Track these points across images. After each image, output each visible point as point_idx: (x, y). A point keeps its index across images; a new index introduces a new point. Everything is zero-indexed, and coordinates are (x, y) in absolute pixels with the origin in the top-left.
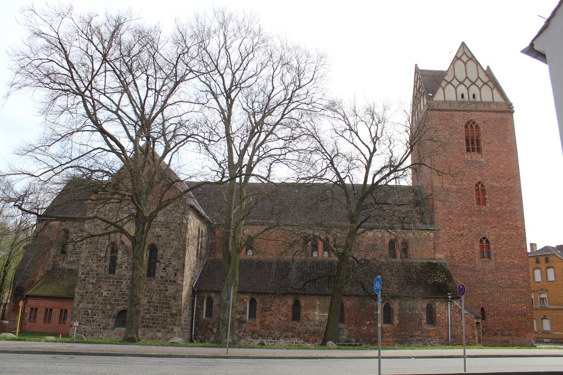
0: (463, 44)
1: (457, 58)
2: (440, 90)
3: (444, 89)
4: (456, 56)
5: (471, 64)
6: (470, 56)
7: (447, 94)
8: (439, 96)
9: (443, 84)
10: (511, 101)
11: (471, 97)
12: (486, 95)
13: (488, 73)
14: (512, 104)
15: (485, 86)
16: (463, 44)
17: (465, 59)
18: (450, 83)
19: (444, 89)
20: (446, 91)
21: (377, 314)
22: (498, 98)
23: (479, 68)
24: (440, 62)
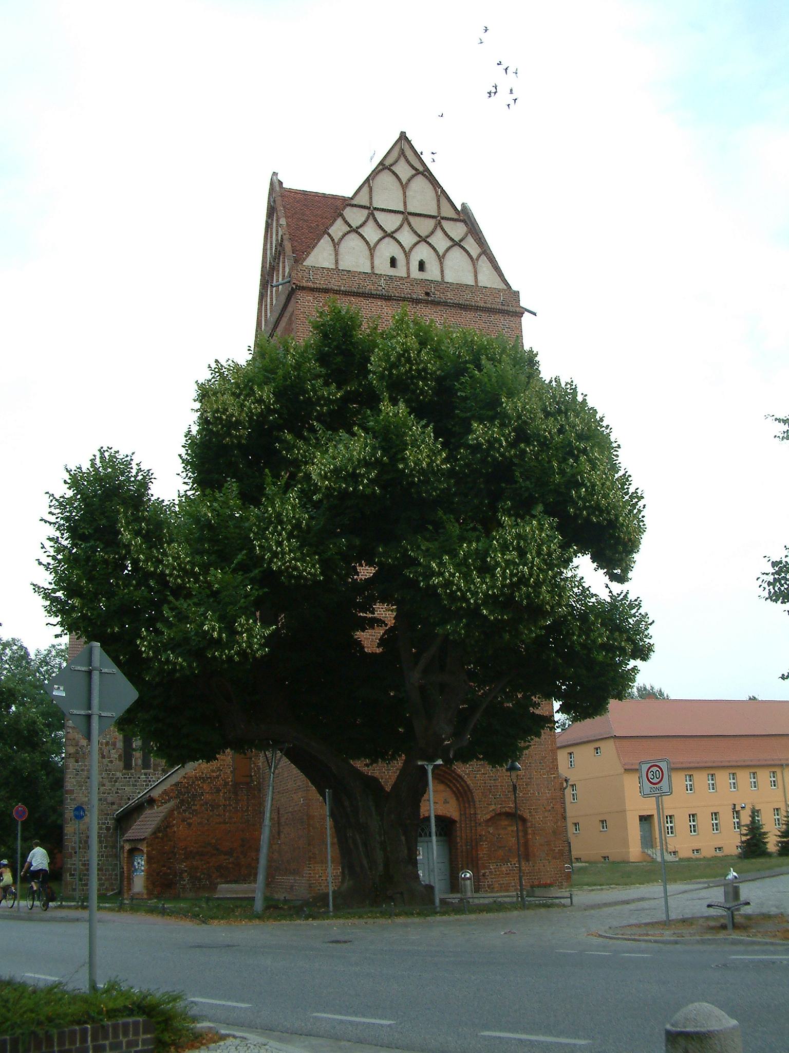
0: (403, 137)
1: (383, 167)
2: (325, 242)
3: (336, 245)
4: (381, 163)
5: (420, 183)
6: (421, 169)
7: (345, 255)
8: (321, 256)
9: (338, 229)
10: (742, 695)
11: (414, 265)
12: (457, 270)
13: (465, 217)
14: (517, 294)
15: (456, 248)
16: (403, 137)
17: (404, 171)
18: (356, 231)
19: (336, 245)
20: (343, 248)
21: (287, 217)
22: (486, 278)
23: (443, 201)
24: (336, 172)
